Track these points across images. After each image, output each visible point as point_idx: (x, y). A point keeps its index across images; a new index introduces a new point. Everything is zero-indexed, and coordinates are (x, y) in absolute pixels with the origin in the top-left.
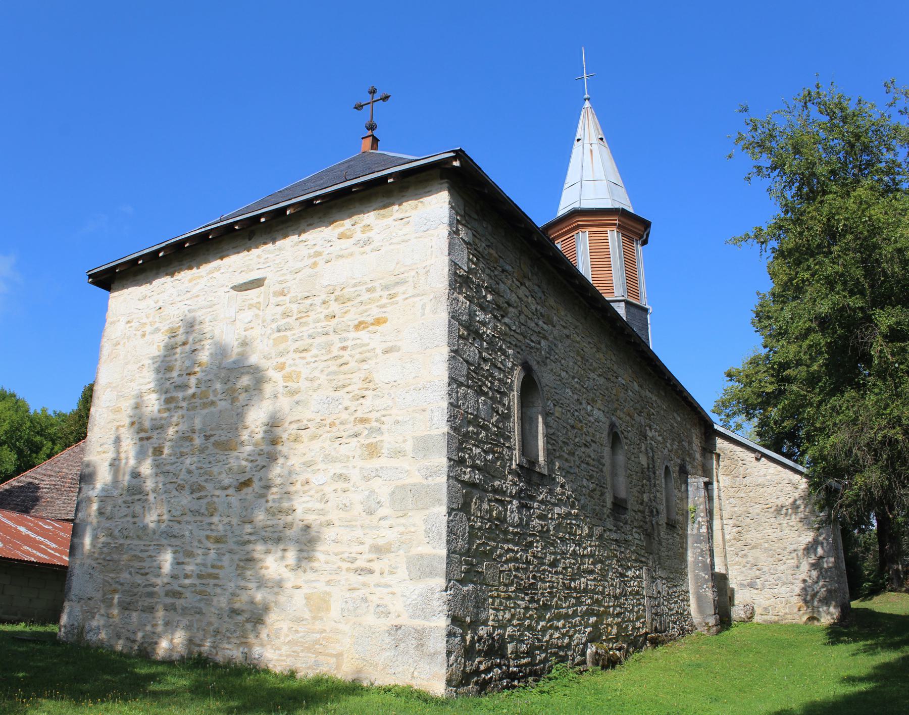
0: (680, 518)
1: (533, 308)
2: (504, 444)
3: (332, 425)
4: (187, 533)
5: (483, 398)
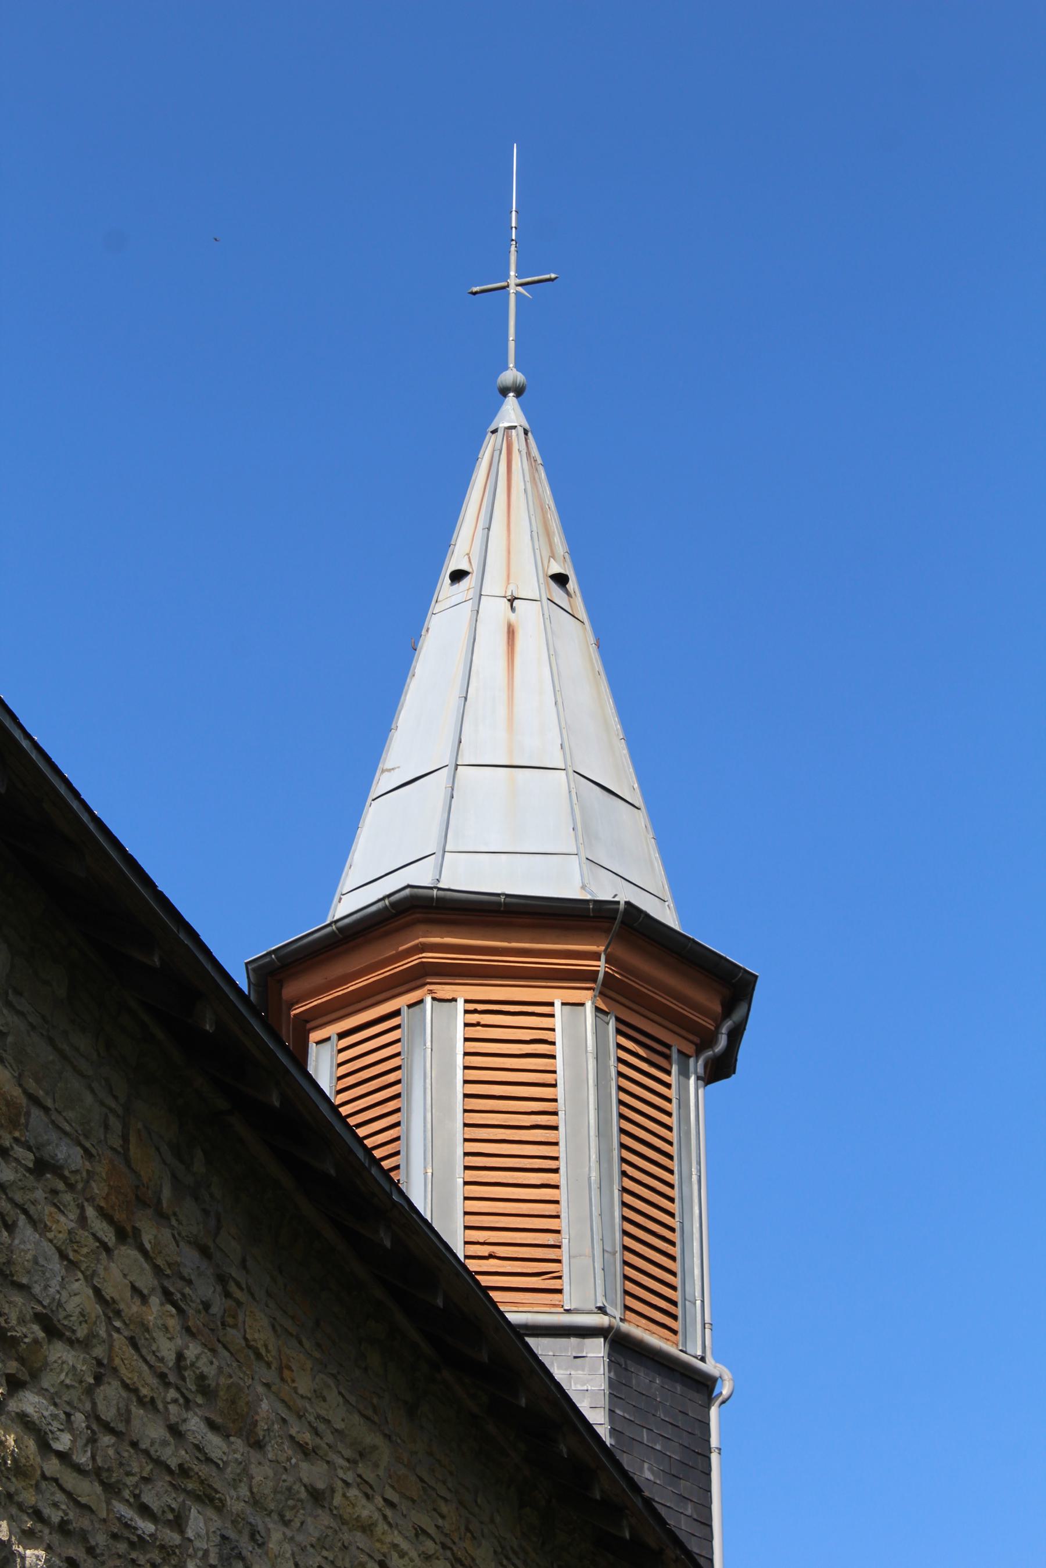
1: (167, 1349)
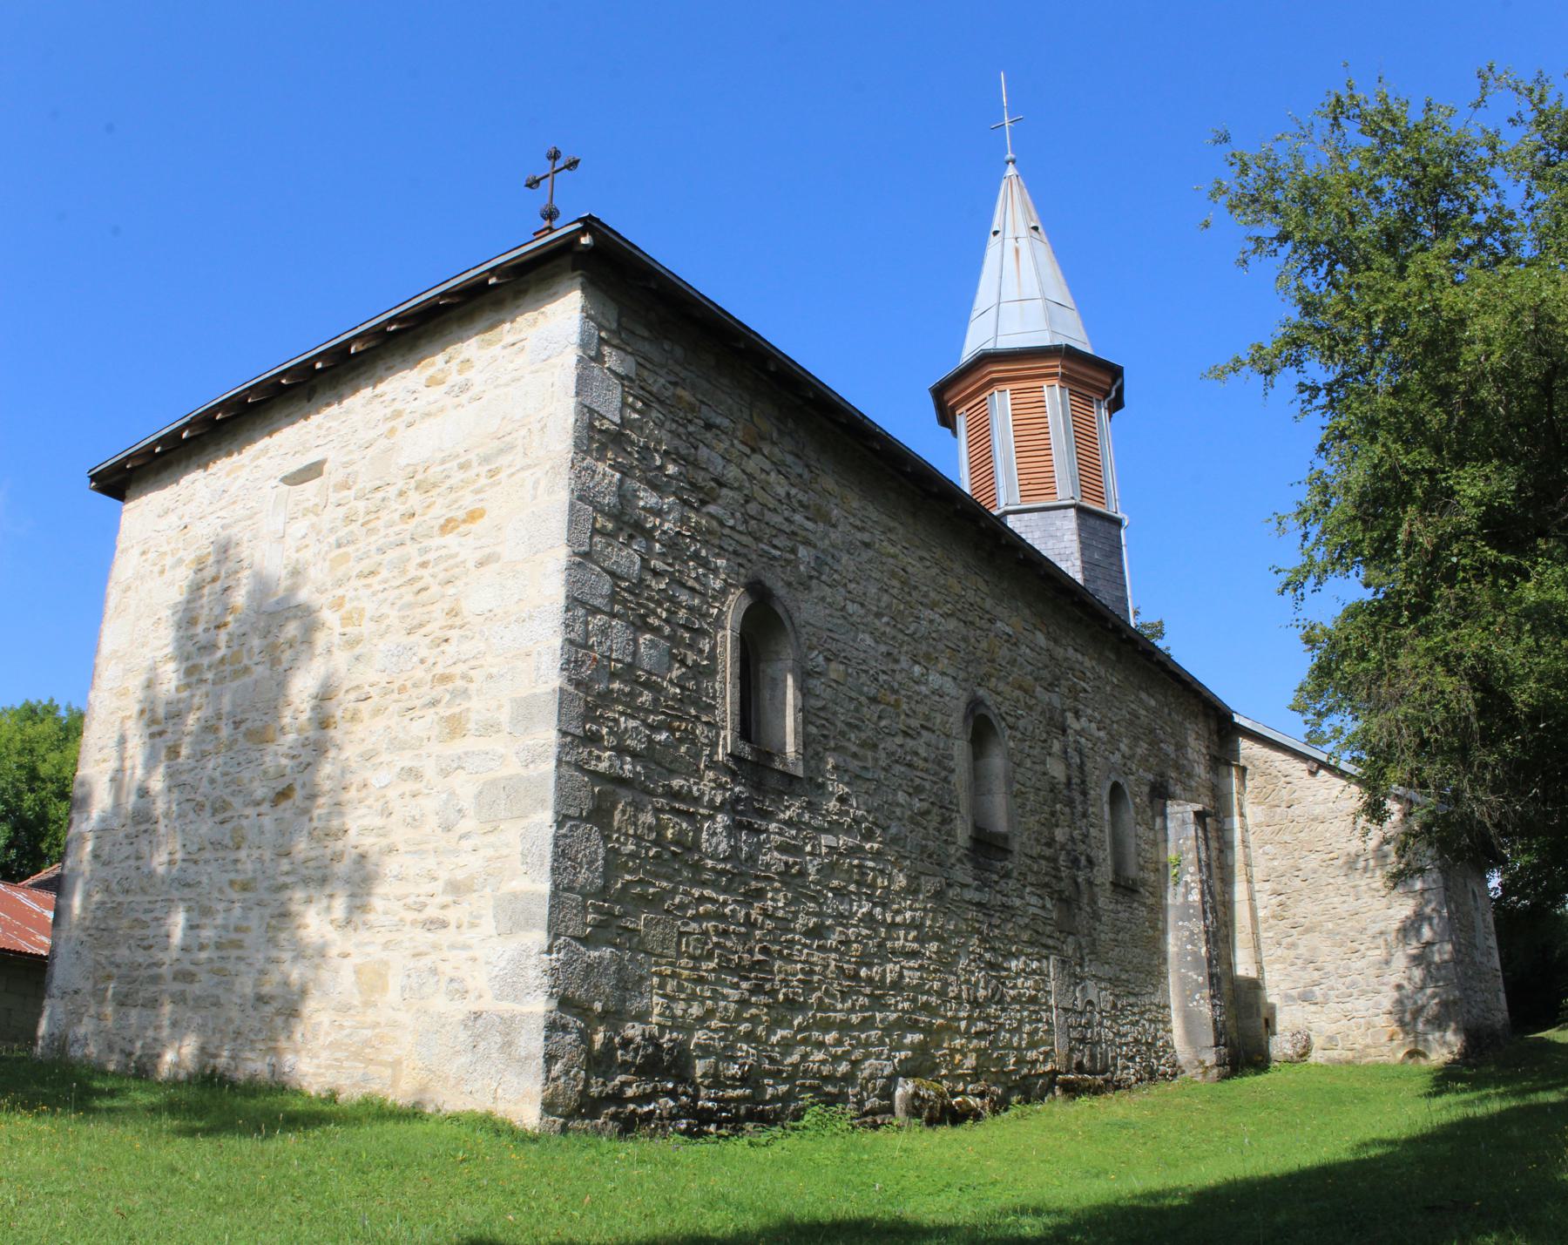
0: (1152, 877)
1: (781, 492)
2: (697, 718)
3: (402, 689)
4: (205, 879)
5: (648, 636)
